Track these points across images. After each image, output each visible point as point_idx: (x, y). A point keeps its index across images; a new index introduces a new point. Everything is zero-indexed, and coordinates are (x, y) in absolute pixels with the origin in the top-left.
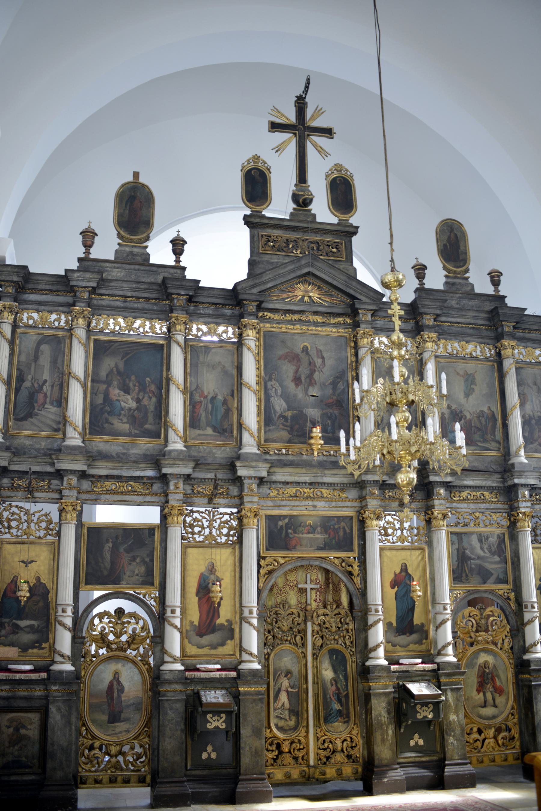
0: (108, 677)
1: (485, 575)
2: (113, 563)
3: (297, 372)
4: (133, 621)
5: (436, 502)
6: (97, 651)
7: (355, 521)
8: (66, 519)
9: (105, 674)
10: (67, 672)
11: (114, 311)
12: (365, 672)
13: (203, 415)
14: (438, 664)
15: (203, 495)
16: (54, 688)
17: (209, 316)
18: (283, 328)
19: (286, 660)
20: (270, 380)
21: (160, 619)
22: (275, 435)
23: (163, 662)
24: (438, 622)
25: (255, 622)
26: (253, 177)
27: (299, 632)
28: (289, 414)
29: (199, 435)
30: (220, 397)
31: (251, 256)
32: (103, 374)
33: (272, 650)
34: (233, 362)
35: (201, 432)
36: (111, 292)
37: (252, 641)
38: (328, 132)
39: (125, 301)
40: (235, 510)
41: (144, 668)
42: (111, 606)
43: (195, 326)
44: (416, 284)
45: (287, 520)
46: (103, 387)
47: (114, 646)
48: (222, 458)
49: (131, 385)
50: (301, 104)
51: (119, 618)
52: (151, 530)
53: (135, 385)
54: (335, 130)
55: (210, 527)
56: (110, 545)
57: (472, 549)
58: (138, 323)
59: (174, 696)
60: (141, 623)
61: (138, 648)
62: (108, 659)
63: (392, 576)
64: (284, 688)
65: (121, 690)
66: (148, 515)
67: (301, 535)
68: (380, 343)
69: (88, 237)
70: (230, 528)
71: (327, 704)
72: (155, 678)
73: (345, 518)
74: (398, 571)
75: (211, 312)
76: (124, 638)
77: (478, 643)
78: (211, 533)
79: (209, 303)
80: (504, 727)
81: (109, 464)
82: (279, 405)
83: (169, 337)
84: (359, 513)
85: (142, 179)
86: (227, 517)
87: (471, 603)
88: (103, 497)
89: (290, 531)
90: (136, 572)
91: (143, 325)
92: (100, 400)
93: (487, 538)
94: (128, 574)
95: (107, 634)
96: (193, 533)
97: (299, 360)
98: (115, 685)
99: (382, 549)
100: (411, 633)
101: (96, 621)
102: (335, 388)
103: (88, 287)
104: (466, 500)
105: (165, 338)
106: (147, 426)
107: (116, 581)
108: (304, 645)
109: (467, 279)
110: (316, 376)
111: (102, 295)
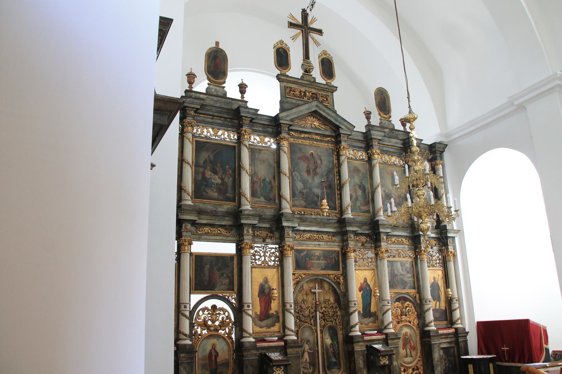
0: (209, 348)
1: (404, 284)
2: (210, 277)
3: (308, 167)
4: (222, 313)
5: (383, 244)
6: (201, 332)
7: (340, 253)
8: (185, 250)
9: (208, 346)
10: (189, 345)
11: (206, 124)
12: (350, 340)
13: (259, 189)
14: (386, 334)
15: (260, 237)
16: (182, 355)
17: (260, 132)
18: (300, 141)
19: (307, 334)
20: (294, 171)
21: (239, 310)
22: (297, 203)
23: (242, 337)
24: (385, 311)
25: (293, 311)
26: (280, 53)
27: (312, 317)
28: (305, 191)
29: (257, 201)
30: (267, 179)
31: (281, 98)
32: (201, 162)
33: (299, 328)
34: (274, 160)
35: (258, 199)
36: (205, 112)
37: (291, 322)
38: (320, 32)
39: (212, 119)
40: (277, 246)
41: (229, 341)
42: (209, 304)
43: (252, 137)
44: (187, 86)
45: (305, 253)
46: (201, 170)
47: (212, 328)
48: (270, 215)
49: (218, 169)
50: (305, 14)
51: (214, 311)
52: (231, 257)
53: (220, 170)
54: (323, 31)
55: (265, 256)
56: (208, 266)
57: (398, 270)
58: (220, 132)
59: (251, 357)
60: (227, 314)
61: (225, 329)
62: (209, 337)
63: (360, 285)
64: (306, 350)
65: (217, 355)
66: (229, 248)
67: (313, 261)
68: (255, 139)
69: (191, 78)
70: (276, 257)
71: (329, 358)
72: (239, 347)
73: (335, 251)
74: (362, 282)
75: (261, 129)
76: (217, 323)
77: (402, 321)
78: (265, 259)
79: (260, 124)
80: (416, 368)
81: (208, 217)
82: (299, 186)
83: (239, 141)
84: (342, 249)
85: (221, 46)
86: (273, 250)
87: (398, 300)
88: (203, 237)
89: (307, 259)
90: (224, 282)
91: (223, 134)
92: (200, 178)
93: (405, 265)
94: (219, 284)
95: (208, 321)
96: (255, 259)
97: (309, 160)
98: (214, 353)
99: (252, 268)
100: (370, 317)
101: (201, 313)
102: (328, 178)
103: (194, 108)
104: (394, 243)
105: (236, 143)
106: (228, 195)
107: (212, 288)
108: (316, 325)
109: (390, 121)
110: (318, 170)
111: (199, 113)
